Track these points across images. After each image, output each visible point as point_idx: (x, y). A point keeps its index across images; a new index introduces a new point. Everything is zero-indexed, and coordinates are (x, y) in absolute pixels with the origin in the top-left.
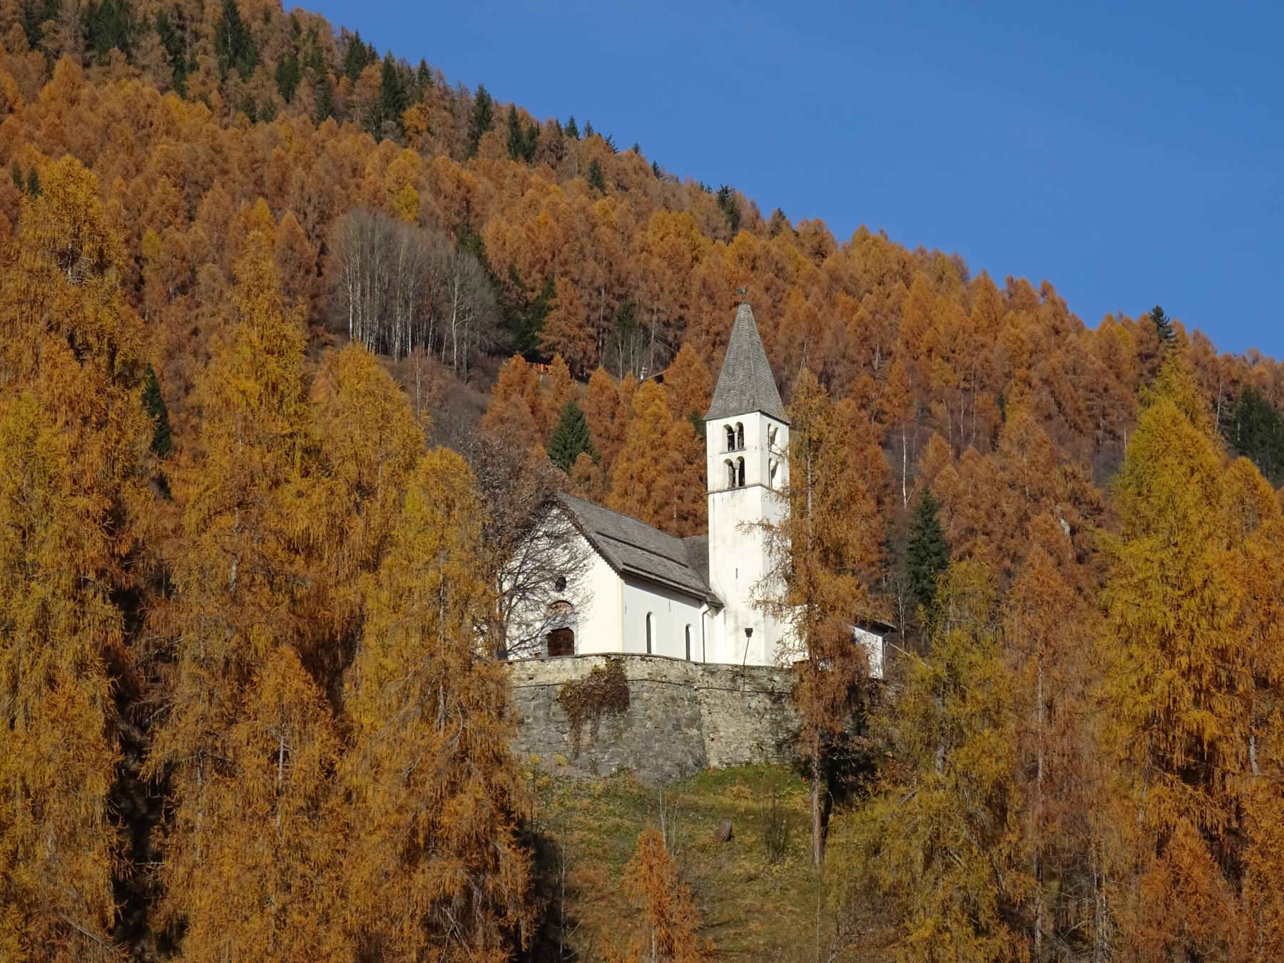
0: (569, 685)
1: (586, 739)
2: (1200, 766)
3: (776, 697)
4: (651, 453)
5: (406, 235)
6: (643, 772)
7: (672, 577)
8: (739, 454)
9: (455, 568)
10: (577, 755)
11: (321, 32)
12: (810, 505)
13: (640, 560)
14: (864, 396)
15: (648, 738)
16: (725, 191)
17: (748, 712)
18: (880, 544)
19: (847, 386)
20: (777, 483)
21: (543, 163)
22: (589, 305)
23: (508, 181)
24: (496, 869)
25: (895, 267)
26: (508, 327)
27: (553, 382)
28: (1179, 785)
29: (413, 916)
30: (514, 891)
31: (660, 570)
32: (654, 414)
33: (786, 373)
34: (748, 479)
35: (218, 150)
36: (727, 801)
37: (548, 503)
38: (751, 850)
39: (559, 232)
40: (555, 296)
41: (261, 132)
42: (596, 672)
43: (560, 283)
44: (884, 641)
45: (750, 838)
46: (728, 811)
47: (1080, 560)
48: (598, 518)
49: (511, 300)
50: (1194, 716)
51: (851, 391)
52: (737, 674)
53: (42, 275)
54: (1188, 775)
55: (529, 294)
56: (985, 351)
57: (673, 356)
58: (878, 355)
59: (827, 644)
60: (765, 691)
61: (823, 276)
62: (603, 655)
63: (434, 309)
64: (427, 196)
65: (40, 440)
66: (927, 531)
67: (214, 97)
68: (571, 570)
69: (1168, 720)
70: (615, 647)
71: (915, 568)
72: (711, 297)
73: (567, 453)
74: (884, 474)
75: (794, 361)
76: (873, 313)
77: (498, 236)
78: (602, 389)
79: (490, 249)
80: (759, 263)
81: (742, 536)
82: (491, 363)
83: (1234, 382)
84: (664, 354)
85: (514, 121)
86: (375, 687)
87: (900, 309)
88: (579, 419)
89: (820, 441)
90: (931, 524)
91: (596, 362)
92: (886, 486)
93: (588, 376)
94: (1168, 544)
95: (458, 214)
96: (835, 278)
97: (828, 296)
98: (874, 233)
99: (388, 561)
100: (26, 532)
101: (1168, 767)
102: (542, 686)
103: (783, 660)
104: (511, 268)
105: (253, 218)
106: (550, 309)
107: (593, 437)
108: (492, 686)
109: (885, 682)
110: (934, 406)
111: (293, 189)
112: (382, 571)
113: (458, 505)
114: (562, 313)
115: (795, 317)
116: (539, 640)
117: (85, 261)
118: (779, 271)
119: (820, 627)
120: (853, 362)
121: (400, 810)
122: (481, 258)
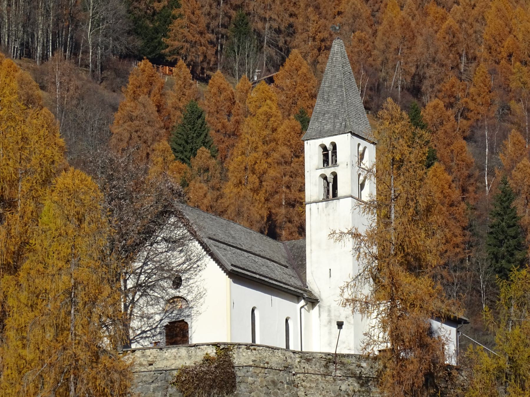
0: (184, 371)
4: (262, 148)
7: (274, 276)
8: (332, 170)
9: (84, 274)
12: (393, 216)
13: (246, 261)
14: (452, 96)
18: (464, 229)
19: (437, 87)
20: (366, 196)
22: (209, 14)
26: (138, 34)
31: (264, 270)
33: (383, 74)
34: (341, 192)
37: (166, 212)
40: (179, 6)
42: (207, 359)
44: (458, 332)
49: (140, 10)
51: (440, 91)
52: (329, 361)
57: (283, 60)
58: (464, 59)
59: (406, 337)
60: (354, 375)
62: (214, 345)
63: (72, 18)
66: (506, 217)
68: (186, 271)
70: (224, 338)
71: (495, 250)
72: (317, 8)
73: (189, 147)
74: (468, 166)
75: (390, 65)
76: (460, 22)
78: (220, 91)
81: (334, 241)
82: (122, 65)
84: (275, 57)
86: (15, 375)
87: (483, 18)
88: (200, 117)
89: (402, 161)
90: (508, 211)
91: (216, 64)
92: (470, 176)
93: (209, 77)
99: (26, 265)
102: (160, 371)
103: (369, 350)
106: (174, 18)
107: (212, 132)
108: (116, 376)
109: (457, 369)
110: (513, 104)
112: (21, 274)
113: (87, 218)
114: (185, 21)
115: (391, 25)
116: (158, 330)
119: (401, 323)
120: (442, 65)
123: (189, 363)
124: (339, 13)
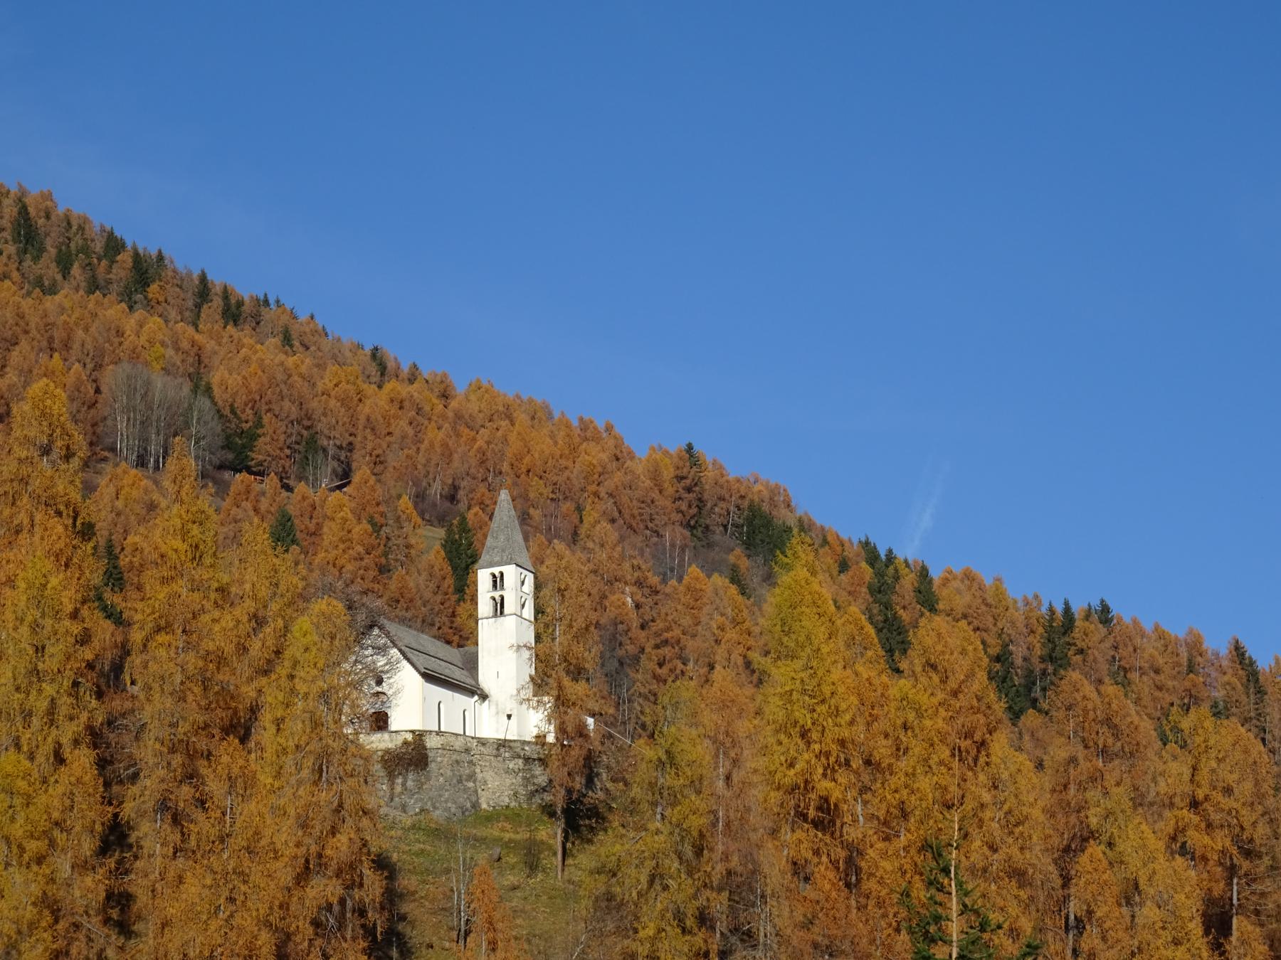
0: (387, 751)
1: (398, 789)
2: (826, 818)
3: (527, 760)
4: (342, 546)
5: (159, 381)
6: (438, 812)
10: (392, 800)
11: (87, 227)
15: (441, 788)
16: (376, 349)
17: (507, 771)
21: (247, 327)
23: (224, 340)
24: (361, 885)
25: (501, 409)
27: (270, 492)
28: (812, 832)
29: (305, 918)
30: (374, 901)
31: (447, 672)
32: (342, 518)
34: (506, 611)
35: (21, 316)
36: (496, 833)
38: (513, 868)
39: (265, 381)
40: (262, 427)
41: (50, 303)
42: (406, 743)
43: (266, 419)
45: (512, 859)
46: (498, 840)
47: (643, 627)
48: (407, 635)
50: (824, 786)
53: (28, 461)
54: (817, 824)
55: (244, 425)
56: (567, 473)
59: (569, 729)
61: (451, 414)
64: (170, 352)
65: (49, 586)
67: (15, 275)
68: (387, 672)
69: (805, 788)
72: (373, 429)
75: (431, 476)
76: (488, 443)
77: (222, 383)
78: (304, 498)
79: (217, 391)
80: (406, 404)
83: (742, 497)
85: (226, 294)
94: (806, 668)
95: (192, 365)
96: (458, 416)
97: (454, 429)
98: (485, 383)
100: (40, 650)
101: (804, 817)
104: (232, 406)
105: (50, 368)
110: (532, 511)
111: (76, 346)
115: (432, 445)
117: (56, 453)
118: (419, 411)
120: (474, 478)
121: (298, 845)
122: (211, 398)
123: (390, 745)
124: (389, 434)
